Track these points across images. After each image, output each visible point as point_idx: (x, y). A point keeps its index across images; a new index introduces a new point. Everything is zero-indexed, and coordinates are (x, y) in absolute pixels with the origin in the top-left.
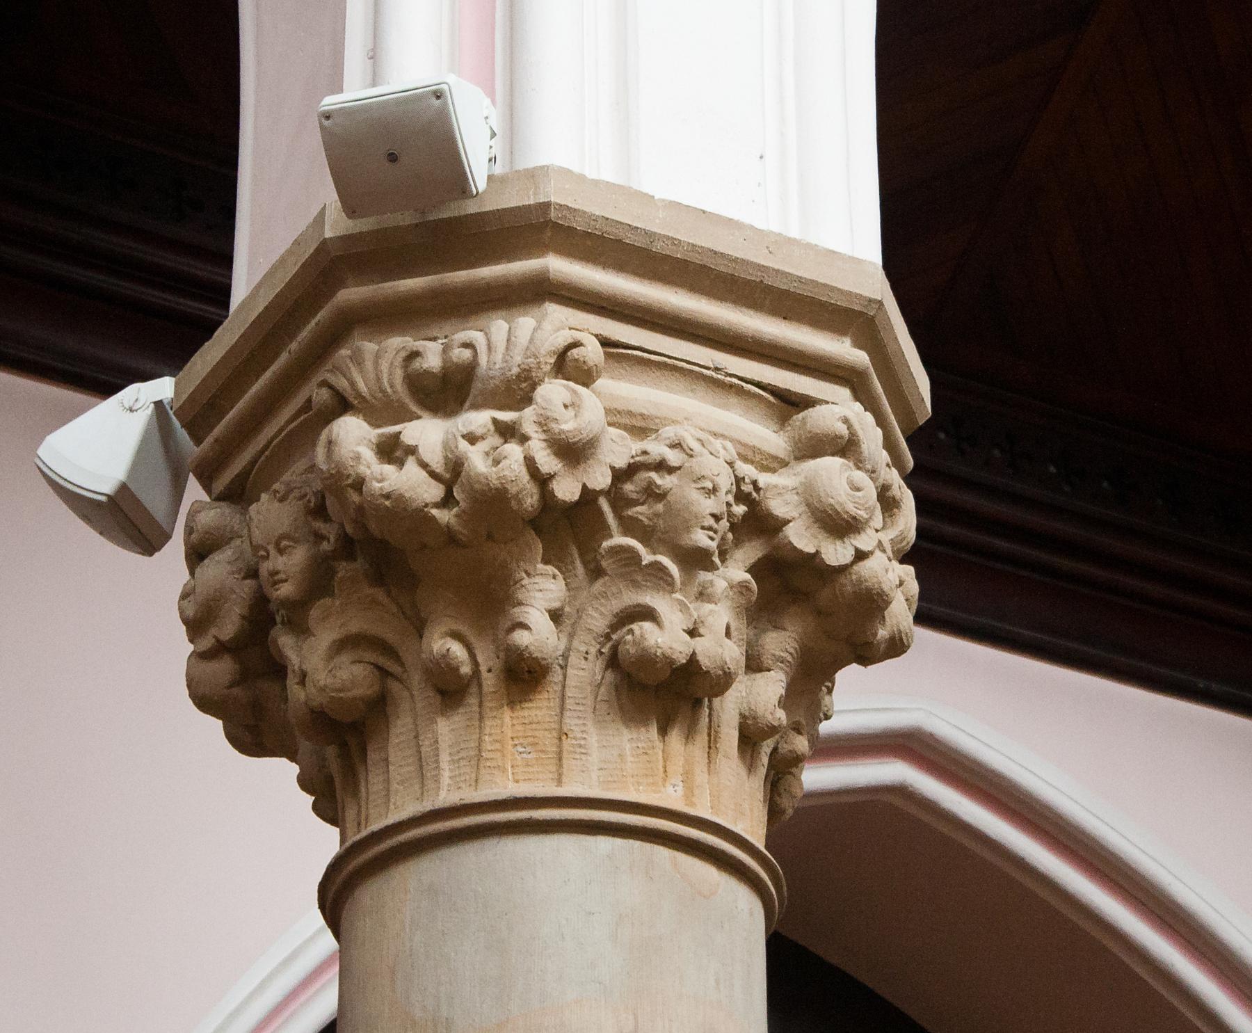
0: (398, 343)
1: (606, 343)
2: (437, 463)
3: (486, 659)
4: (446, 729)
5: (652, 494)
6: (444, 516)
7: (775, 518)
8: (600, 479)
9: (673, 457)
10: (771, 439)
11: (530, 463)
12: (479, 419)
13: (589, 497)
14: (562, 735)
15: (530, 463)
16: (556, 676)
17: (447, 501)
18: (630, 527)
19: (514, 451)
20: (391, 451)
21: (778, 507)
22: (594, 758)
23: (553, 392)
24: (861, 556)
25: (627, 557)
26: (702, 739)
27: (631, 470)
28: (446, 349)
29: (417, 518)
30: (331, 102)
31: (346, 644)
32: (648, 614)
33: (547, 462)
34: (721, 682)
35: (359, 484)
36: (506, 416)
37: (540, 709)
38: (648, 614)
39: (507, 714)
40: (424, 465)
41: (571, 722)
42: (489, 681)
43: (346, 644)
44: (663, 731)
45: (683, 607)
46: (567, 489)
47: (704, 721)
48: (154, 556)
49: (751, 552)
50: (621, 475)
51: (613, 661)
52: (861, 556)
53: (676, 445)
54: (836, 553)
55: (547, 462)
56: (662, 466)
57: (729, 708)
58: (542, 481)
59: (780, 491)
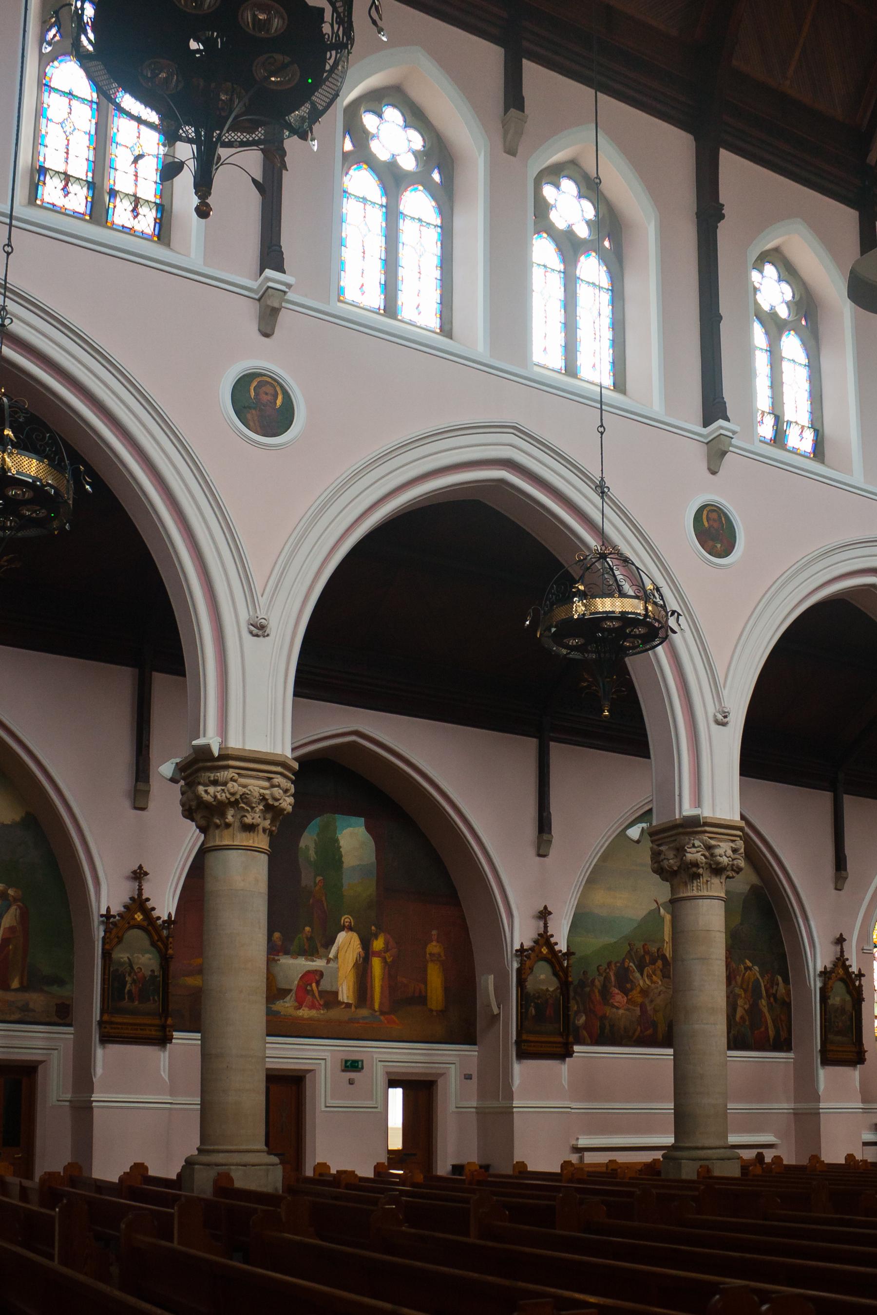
0: (208, 774)
1: (238, 774)
2: (213, 796)
3: (222, 822)
4: (217, 832)
5: (246, 798)
6: (214, 803)
7: (788, 307)
8: (238, 797)
9: (249, 792)
10: (266, 784)
11: (226, 797)
12: (219, 788)
13: (236, 800)
14: (234, 834)
15: (226, 797)
16: (233, 825)
17: (215, 801)
18: (244, 803)
19: (224, 795)
20: (206, 791)
21: (267, 797)
22: (238, 838)
23: (230, 785)
24: (280, 804)
25: (243, 808)
26: (256, 833)
27: (243, 794)
28: (214, 776)
29: (210, 803)
30: (194, 743)
31: (202, 817)
32: (246, 816)
33: (228, 796)
34: (258, 825)
35: (202, 798)
36: (223, 788)
37: (231, 829)
38: (246, 816)
39: (226, 830)
40: (211, 796)
41: (235, 832)
42: (223, 825)
43: (202, 817)
44: (249, 832)
45: (251, 815)
46: (233, 799)
47: (256, 830)
48: (330, 1165)
49: (263, 803)
50: (241, 796)
51: (241, 822)
52: (280, 804)
53: (250, 790)
54: (276, 804)
55: (228, 796)
56: (248, 794)
57: (260, 828)
58: (229, 799)
59: (267, 794)
